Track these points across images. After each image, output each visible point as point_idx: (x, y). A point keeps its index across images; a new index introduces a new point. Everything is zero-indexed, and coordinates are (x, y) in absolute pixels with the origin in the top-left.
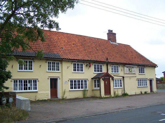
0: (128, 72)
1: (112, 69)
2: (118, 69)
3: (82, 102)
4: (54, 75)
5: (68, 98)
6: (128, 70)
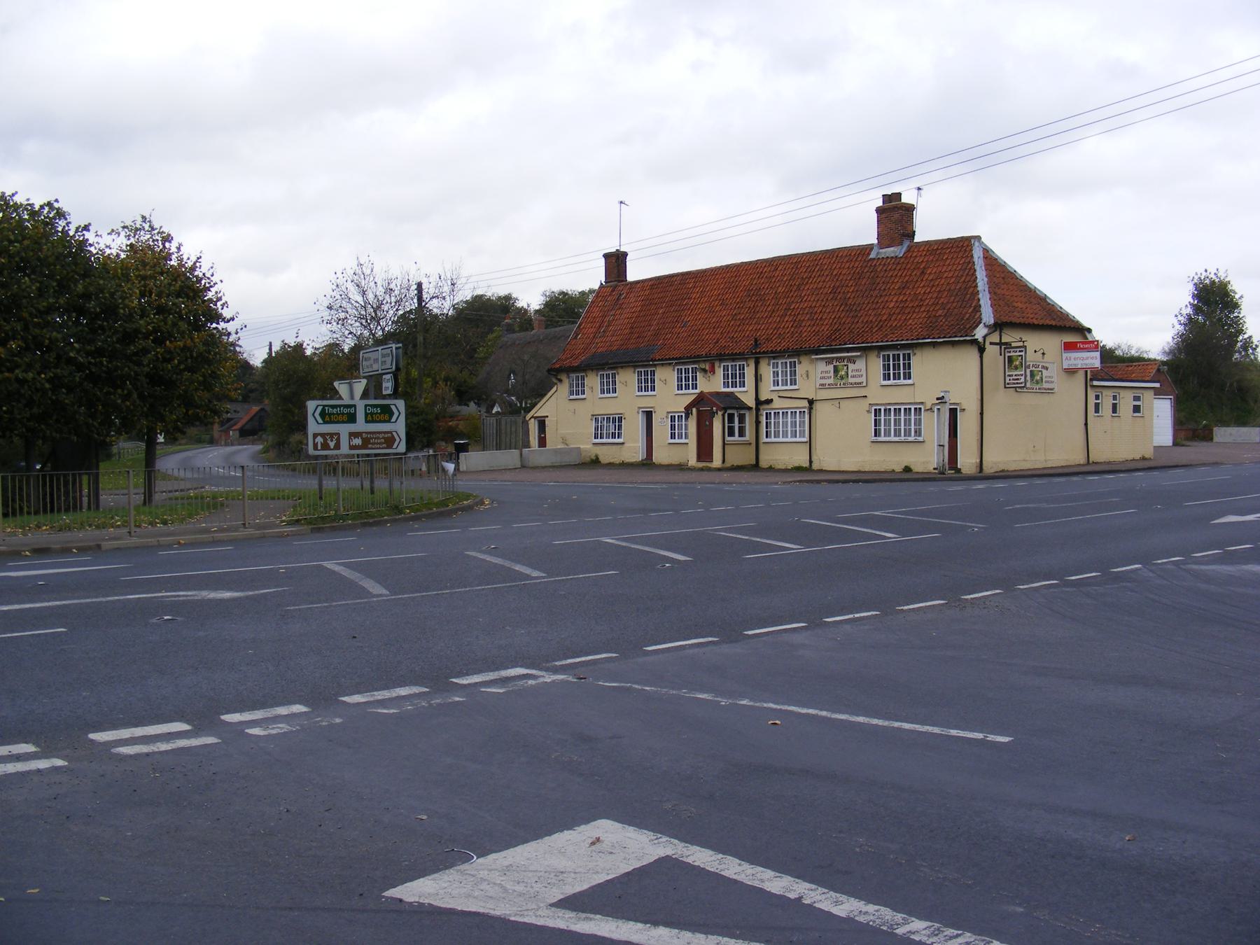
0: (831, 381)
1: (776, 374)
2: (794, 373)
3: (1001, 467)
4: (647, 403)
5: (665, 461)
6: (832, 374)
